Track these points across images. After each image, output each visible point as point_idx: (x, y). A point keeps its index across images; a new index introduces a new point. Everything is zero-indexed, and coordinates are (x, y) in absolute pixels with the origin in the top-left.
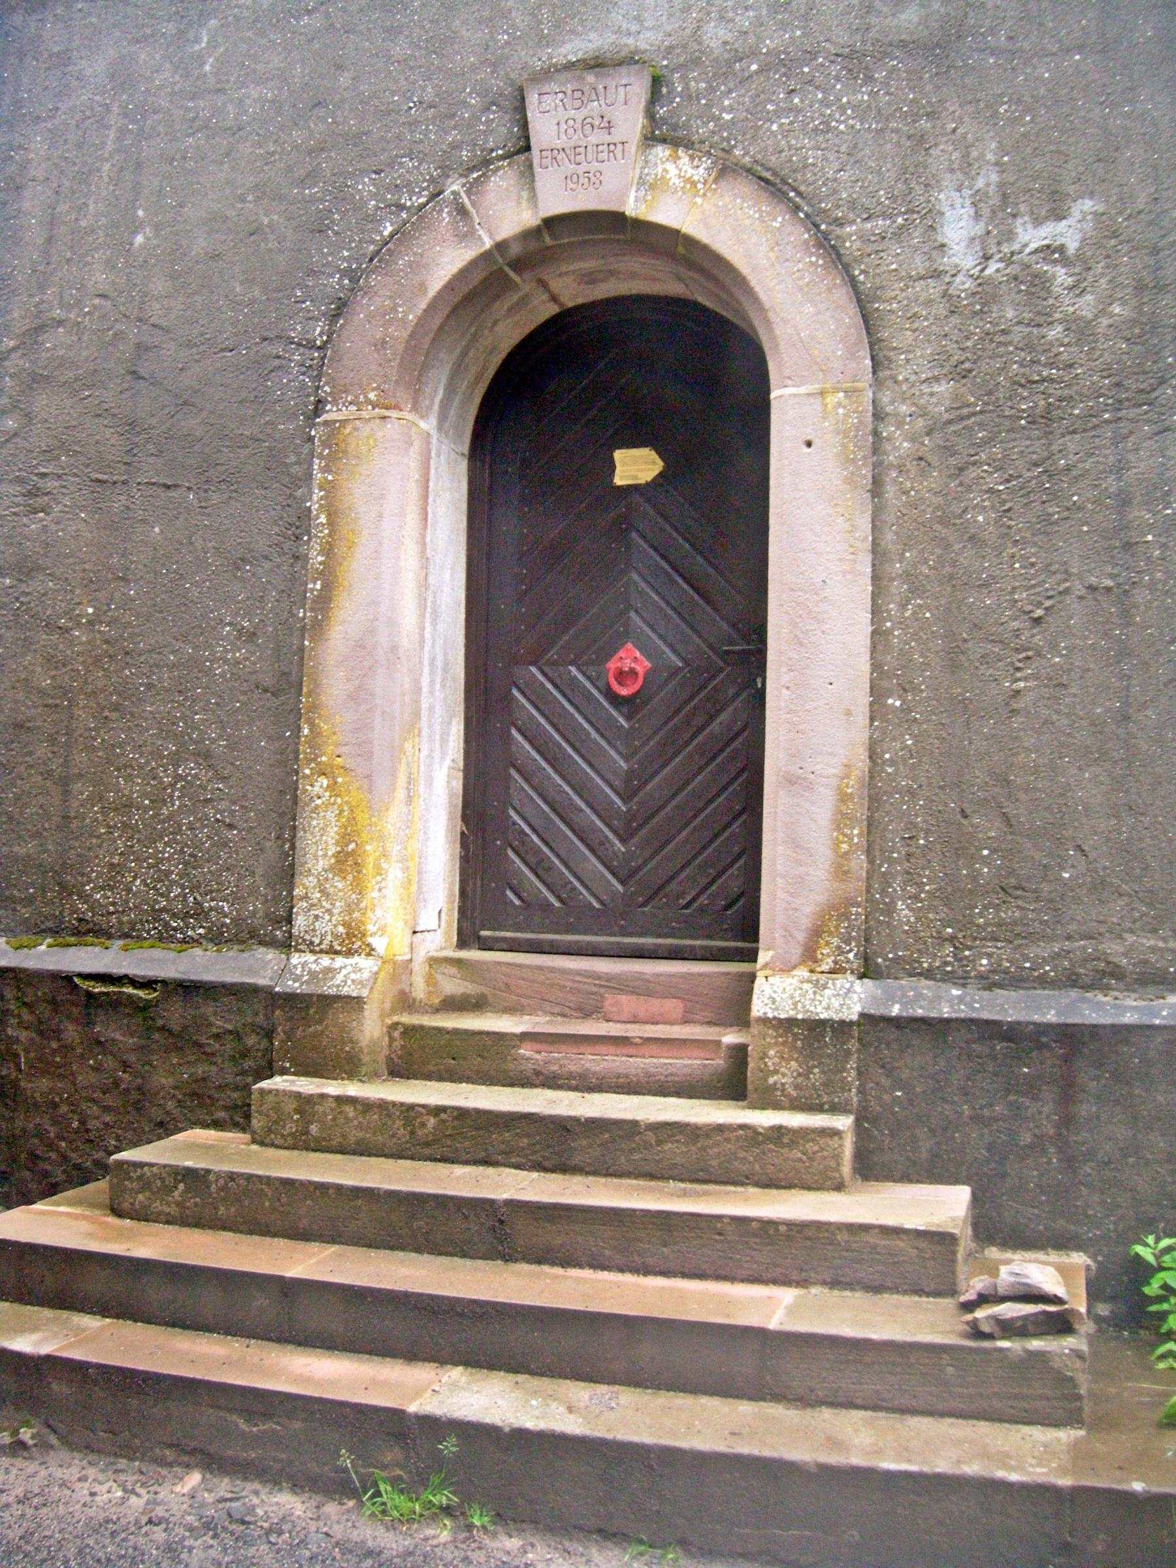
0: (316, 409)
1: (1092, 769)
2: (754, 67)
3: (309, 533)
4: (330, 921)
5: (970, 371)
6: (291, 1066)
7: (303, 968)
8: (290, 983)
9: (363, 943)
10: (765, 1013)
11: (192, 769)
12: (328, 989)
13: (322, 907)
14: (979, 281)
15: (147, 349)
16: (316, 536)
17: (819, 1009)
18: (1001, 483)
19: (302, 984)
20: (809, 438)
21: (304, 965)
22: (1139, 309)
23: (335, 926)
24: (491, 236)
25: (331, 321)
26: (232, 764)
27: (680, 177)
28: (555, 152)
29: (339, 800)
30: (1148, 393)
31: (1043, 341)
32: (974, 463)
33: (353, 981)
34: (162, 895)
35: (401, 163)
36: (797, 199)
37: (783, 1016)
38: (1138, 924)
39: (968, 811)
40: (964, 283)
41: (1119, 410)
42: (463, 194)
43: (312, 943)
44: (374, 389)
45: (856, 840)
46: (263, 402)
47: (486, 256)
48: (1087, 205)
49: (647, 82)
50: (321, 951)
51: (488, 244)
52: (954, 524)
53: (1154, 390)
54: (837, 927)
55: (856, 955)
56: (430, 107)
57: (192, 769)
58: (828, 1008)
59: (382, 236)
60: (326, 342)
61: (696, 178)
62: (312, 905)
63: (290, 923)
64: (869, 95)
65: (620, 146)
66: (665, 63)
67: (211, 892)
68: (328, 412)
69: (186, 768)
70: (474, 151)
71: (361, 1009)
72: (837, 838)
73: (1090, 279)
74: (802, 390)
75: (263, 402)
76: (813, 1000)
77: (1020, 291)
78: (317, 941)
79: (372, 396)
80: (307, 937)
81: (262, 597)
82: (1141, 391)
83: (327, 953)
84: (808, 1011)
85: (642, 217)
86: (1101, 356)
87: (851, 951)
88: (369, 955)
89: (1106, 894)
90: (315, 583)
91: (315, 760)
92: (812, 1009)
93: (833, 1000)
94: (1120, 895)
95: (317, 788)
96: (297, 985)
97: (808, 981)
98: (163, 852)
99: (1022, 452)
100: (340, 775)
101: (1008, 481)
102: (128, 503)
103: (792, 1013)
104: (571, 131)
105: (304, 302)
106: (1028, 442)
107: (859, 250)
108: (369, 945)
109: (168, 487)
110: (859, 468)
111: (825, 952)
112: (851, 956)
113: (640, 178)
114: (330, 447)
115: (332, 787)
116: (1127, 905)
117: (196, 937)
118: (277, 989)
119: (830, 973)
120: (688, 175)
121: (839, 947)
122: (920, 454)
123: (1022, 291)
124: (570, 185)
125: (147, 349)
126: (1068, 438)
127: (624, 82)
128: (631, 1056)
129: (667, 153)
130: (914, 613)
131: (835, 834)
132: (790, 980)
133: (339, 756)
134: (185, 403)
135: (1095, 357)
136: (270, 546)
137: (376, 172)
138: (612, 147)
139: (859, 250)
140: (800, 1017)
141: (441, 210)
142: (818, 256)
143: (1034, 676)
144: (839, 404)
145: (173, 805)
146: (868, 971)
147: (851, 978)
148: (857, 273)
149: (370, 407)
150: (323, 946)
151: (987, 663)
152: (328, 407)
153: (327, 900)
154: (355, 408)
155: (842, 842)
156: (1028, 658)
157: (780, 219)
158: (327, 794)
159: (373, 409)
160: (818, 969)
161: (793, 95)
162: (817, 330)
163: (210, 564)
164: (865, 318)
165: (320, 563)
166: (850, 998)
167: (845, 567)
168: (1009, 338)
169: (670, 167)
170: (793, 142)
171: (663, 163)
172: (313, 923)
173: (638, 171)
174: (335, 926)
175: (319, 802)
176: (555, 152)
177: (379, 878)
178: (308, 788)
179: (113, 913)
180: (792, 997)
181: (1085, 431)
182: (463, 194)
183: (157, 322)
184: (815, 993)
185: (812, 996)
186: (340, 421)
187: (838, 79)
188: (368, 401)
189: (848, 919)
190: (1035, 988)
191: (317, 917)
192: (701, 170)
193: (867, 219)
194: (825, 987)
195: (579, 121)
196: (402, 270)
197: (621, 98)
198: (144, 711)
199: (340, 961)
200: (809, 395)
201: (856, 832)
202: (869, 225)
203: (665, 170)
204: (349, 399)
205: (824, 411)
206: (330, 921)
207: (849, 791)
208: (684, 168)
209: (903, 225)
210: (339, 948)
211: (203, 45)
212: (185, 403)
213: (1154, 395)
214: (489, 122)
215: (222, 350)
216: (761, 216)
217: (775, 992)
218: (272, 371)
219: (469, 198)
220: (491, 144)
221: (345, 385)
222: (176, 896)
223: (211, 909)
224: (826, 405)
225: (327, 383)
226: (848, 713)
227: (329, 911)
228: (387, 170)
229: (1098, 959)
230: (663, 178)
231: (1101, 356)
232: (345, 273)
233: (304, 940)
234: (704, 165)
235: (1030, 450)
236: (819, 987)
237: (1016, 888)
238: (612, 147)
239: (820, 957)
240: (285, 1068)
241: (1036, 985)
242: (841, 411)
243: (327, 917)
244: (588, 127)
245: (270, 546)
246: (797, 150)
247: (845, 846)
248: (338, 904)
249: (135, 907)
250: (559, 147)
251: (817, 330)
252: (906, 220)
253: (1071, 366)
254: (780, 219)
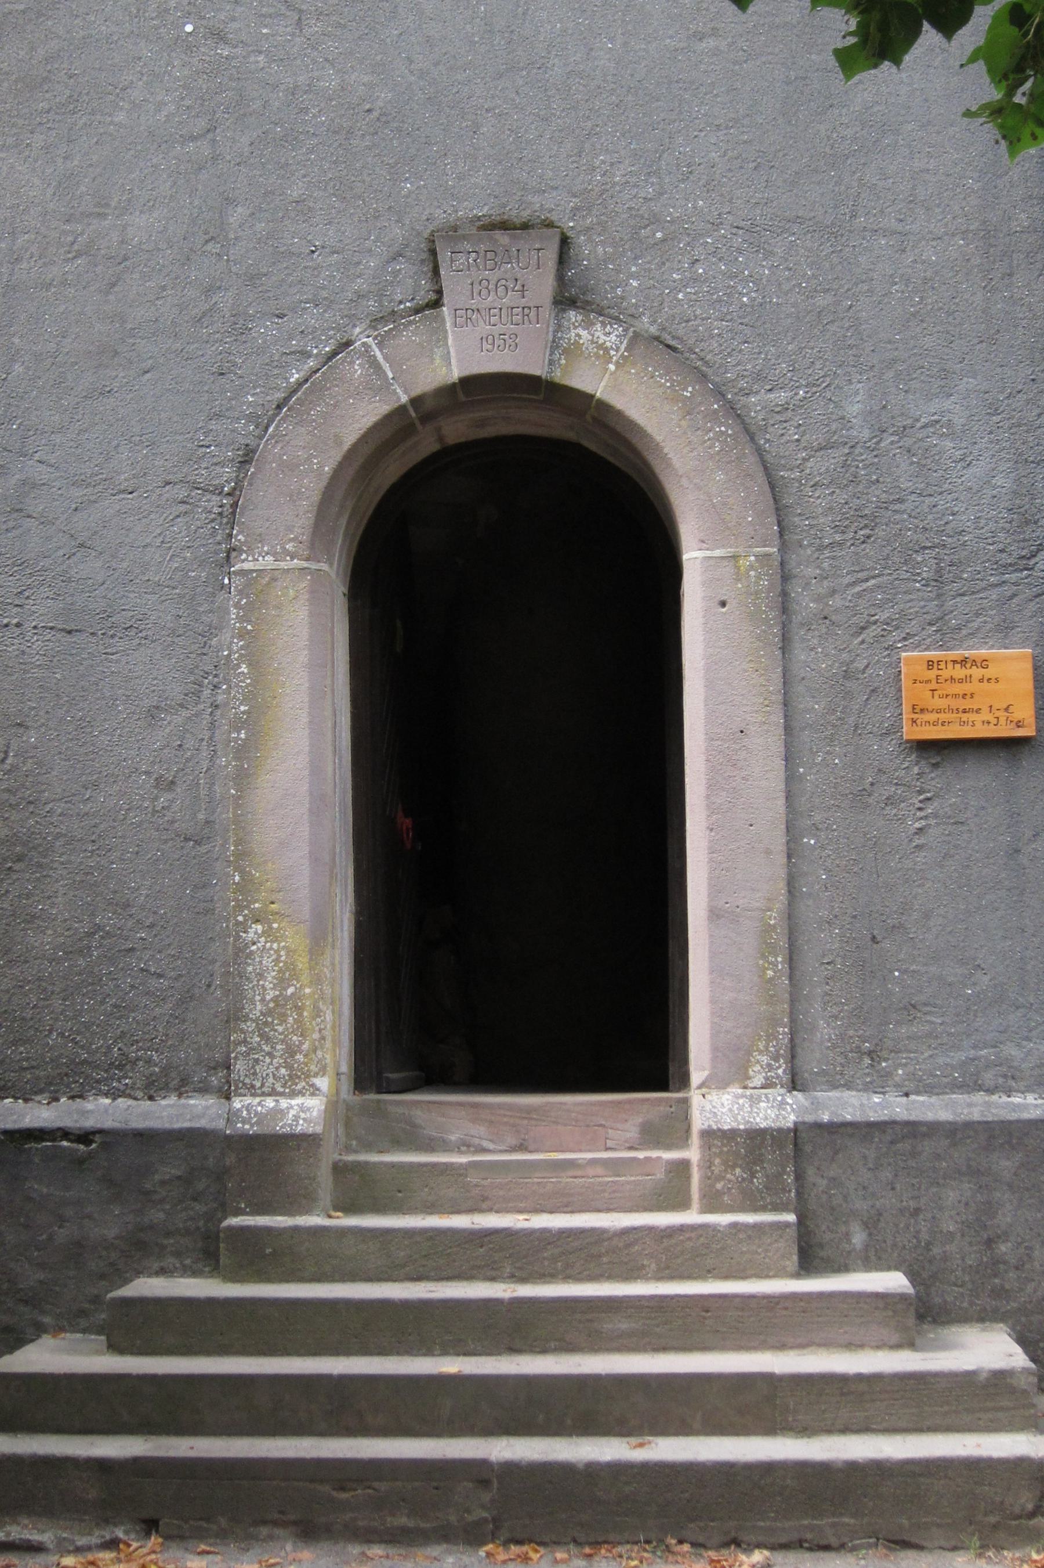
0: (228, 557)
1: (988, 897)
2: (659, 235)
3: (227, 681)
4: (271, 1063)
5: (869, 537)
6: (246, 1207)
7: (247, 1110)
8: (239, 1125)
9: (307, 1083)
10: (709, 1126)
11: (110, 919)
12: (281, 1127)
13: (262, 1050)
14: (875, 453)
15: (34, 486)
16: (237, 686)
17: (758, 1120)
18: (900, 641)
19: (252, 1126)
20: (724, 598)
21: (248, 1108)
22: (1018, 481)
23: (277, 1068)
24: (405, 392)
25: (239, 468)
26: (155, 913)
27: (592, 342)
28: (469, 311)
29: (275, 946)
30: (1029, 558)
31: (935, 510)
32: (875, 622)
33: (304, 1119)
34: (82, 1047)
35: (306, 309)
36: (704, 368)
37: (726, 1127)
38: (1034, 1033)
39: (879, 938)
40: (862, 455)
41: (1003, 574)
42: (374, 347)
43: (253, 1086)
44: (291, 540)
45: (780, 967)
46: (170, 548)
47: (401, 410)
48: (969, 383)
49: (557, 240)
50: (263, 1094)
51: (404, 399)
52: (858, 679)
53: (1034, 556)
54: (767, 1047)
55: (784, 1070)
56: (334, 252)
57: (110, 919)
58: (766, 1119)
59: (288, 382)
60: (234, 489)
61: (608, 344)
62: (252, 1049)
63: (228, 1068)
64: (769, 269)
65: (534, 310)
66: (571, 224)
67: (137, 1042)
68: (243, 561)
69: (103, 917)
70: (380, 302)
71: (319, 1146)
72: (763, 966)
73: (976, 453)
74: (718, 553)
75: (170, 548)
76: (750, 1112)
77: (912, 463)
78: (258, 1084)
79: (289, 546)
80: (247, 1081)
81: (180, 746)
82: (1023, 557)
83: (270, 1095)
84: (748, 1122)
85: (557, 380)
86: (987, 524)
87: (779, 1067)
88: (313, 1094)
89: (1005, 1006)
90: (239, 733)
91: (247, 907)
92: (752, 1120)
93: (769, 1111)
94: (1018, 1008)
95: (251, 935)
96: (247, 1127)
97: (743, 1096)
98: (82, 1004)
99: (917, 612)
100: (275, 921)
101: (905, 639)
102: (23, 647)
103: (734, 1125)
104: (484, 292)
105: (209, 447)
106: (922, 603)
107: (764, 420)
108: (313, 1085)
109: (70, 632)
110: (770, 627)
111: (755, 1069)
112: (780, 1071)
113: (554, 341)
114: (248, 597)
115: (267, 933)
116: (1025, 1016)
117: (122, 1088)
118: (228, 1132)
119: (762, 1088)
120: (601, 341)
121: (769, 1065)
122: (825, 613)
123: (914, 463)
124: (486, 346)
125: (34, 486)
126: (958, 599)
127: (537, 246)
128: (575, 1177)
129: (580, 318)
130: (824, 759)
131: (761, 962)
132: (726, 1096)
133: (273, 903)
134: (81, 545)
135: (981, 525)
136: (186, 695)
137: (278, 317)
138: (526, 311)
139: (764, 420)
140: (742, 1127)
141: (352, 363)
142: (727, 427)
143: (935, 815)
144: (751, 567)
145: (91, 956)
146: (794, 1084)
147: (783, 1091)
148: (762, 442)
149: (288, 558)
150: (265, 1089)
151: (892, 804)
152: (244, 556)
153: (267, 1043)
154: (272, 558)
155: (768, 969)
156: (928, 799)
157: (690, 389)
158: (263, 939)
159: (292, 559)
160: (751, 1085)
161: (697, 266)
162: (728, 497)
163: (120, 712)
164: (772, 486)
165: (243, 713)
166: (784, 1109)
167: (760, 718)
168: (903, 507)
169: (584, 333)
170: (698, 312)
171: (575, 328)
172: (253, 1067)
173: (551, 334)
174: (277, 1068)
175: (254, 948)
176: (469, 311)
177: (319, 1020)
178: (244, 935)
179: (27, 1069)
180: (730, 1110)
181: (973, 593)
182: (374, 347)
183: (45, 458)
184: (751, 1106)
185: (749, 1109)
186: (256, 571)
187: (740, 251)
188: (287, 552)
189: (776, 1038)
190: (947, 1093)
191: (257, 1061)
192: (613, 338)
193: (770, 390)
194: (759, 1100)
195: (493, 282)
196: (314, 421)
197: (534, 262)
198: (52, 861)
199: (284, 1103)
200: (722, 558)
201: (780, 959)
202: (772, 396)
203: (578, 335)
204: (266, 549)
205: (737, 574)
206: (271, 1063)
207: (772, 922)
208: (597, 334)
209: (805, 398)
210: (282, 1090)
211: (76, 163)
212: (81, 545)
213: (1032, 562)
214: (396, 273)
215: (123, 491)
216: (672, 385)
217: (714, 1107)
218: (178, 516)
219: (381, 351)
220: (399, 297)
221: (260, 535)
222: (98, 1048)
223: (138, 1059)
224: (739, 568)
225: (239, 532)
226: (768, 852)
227: (270, 1055)
228: (290, 314)
229: (1001, 1065)
230: (576, 343)
231: (987, 524)
232: (251, 418)
233: (244, 1084)
234: (616, 333)
235: (924, 610)
236: (754, 1101)
237: (925, 1005)
238: (526, 311)
239: (751, 1073)
240: (241, 1208)
241: (947, 1090)
242: (752, 573)
243: (268, 1060)
244: (501, 289)
245: (186, 695)
246: (703, 319)
247: (770, 973)
248: (279, 1047)
249: (52, 1060)
250: (473, 307)
251: (728, 497)
252: (807, 392)
253: (960, 533)
254: (690, 389)
